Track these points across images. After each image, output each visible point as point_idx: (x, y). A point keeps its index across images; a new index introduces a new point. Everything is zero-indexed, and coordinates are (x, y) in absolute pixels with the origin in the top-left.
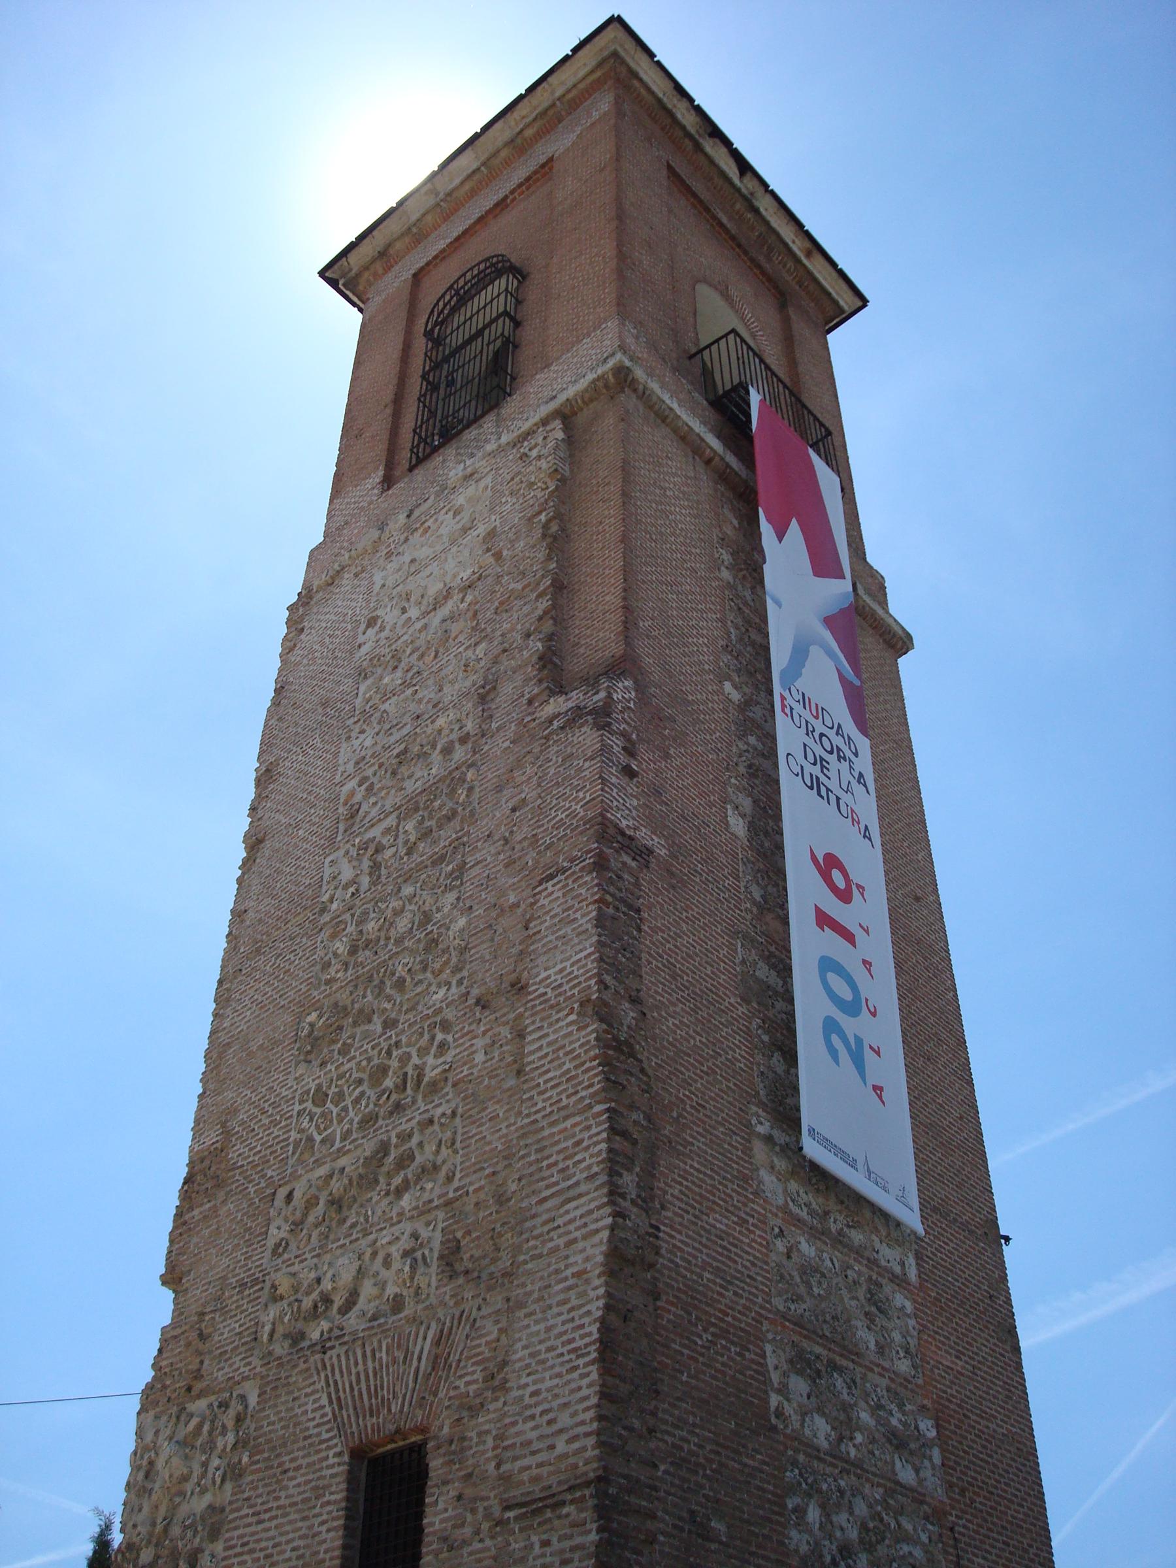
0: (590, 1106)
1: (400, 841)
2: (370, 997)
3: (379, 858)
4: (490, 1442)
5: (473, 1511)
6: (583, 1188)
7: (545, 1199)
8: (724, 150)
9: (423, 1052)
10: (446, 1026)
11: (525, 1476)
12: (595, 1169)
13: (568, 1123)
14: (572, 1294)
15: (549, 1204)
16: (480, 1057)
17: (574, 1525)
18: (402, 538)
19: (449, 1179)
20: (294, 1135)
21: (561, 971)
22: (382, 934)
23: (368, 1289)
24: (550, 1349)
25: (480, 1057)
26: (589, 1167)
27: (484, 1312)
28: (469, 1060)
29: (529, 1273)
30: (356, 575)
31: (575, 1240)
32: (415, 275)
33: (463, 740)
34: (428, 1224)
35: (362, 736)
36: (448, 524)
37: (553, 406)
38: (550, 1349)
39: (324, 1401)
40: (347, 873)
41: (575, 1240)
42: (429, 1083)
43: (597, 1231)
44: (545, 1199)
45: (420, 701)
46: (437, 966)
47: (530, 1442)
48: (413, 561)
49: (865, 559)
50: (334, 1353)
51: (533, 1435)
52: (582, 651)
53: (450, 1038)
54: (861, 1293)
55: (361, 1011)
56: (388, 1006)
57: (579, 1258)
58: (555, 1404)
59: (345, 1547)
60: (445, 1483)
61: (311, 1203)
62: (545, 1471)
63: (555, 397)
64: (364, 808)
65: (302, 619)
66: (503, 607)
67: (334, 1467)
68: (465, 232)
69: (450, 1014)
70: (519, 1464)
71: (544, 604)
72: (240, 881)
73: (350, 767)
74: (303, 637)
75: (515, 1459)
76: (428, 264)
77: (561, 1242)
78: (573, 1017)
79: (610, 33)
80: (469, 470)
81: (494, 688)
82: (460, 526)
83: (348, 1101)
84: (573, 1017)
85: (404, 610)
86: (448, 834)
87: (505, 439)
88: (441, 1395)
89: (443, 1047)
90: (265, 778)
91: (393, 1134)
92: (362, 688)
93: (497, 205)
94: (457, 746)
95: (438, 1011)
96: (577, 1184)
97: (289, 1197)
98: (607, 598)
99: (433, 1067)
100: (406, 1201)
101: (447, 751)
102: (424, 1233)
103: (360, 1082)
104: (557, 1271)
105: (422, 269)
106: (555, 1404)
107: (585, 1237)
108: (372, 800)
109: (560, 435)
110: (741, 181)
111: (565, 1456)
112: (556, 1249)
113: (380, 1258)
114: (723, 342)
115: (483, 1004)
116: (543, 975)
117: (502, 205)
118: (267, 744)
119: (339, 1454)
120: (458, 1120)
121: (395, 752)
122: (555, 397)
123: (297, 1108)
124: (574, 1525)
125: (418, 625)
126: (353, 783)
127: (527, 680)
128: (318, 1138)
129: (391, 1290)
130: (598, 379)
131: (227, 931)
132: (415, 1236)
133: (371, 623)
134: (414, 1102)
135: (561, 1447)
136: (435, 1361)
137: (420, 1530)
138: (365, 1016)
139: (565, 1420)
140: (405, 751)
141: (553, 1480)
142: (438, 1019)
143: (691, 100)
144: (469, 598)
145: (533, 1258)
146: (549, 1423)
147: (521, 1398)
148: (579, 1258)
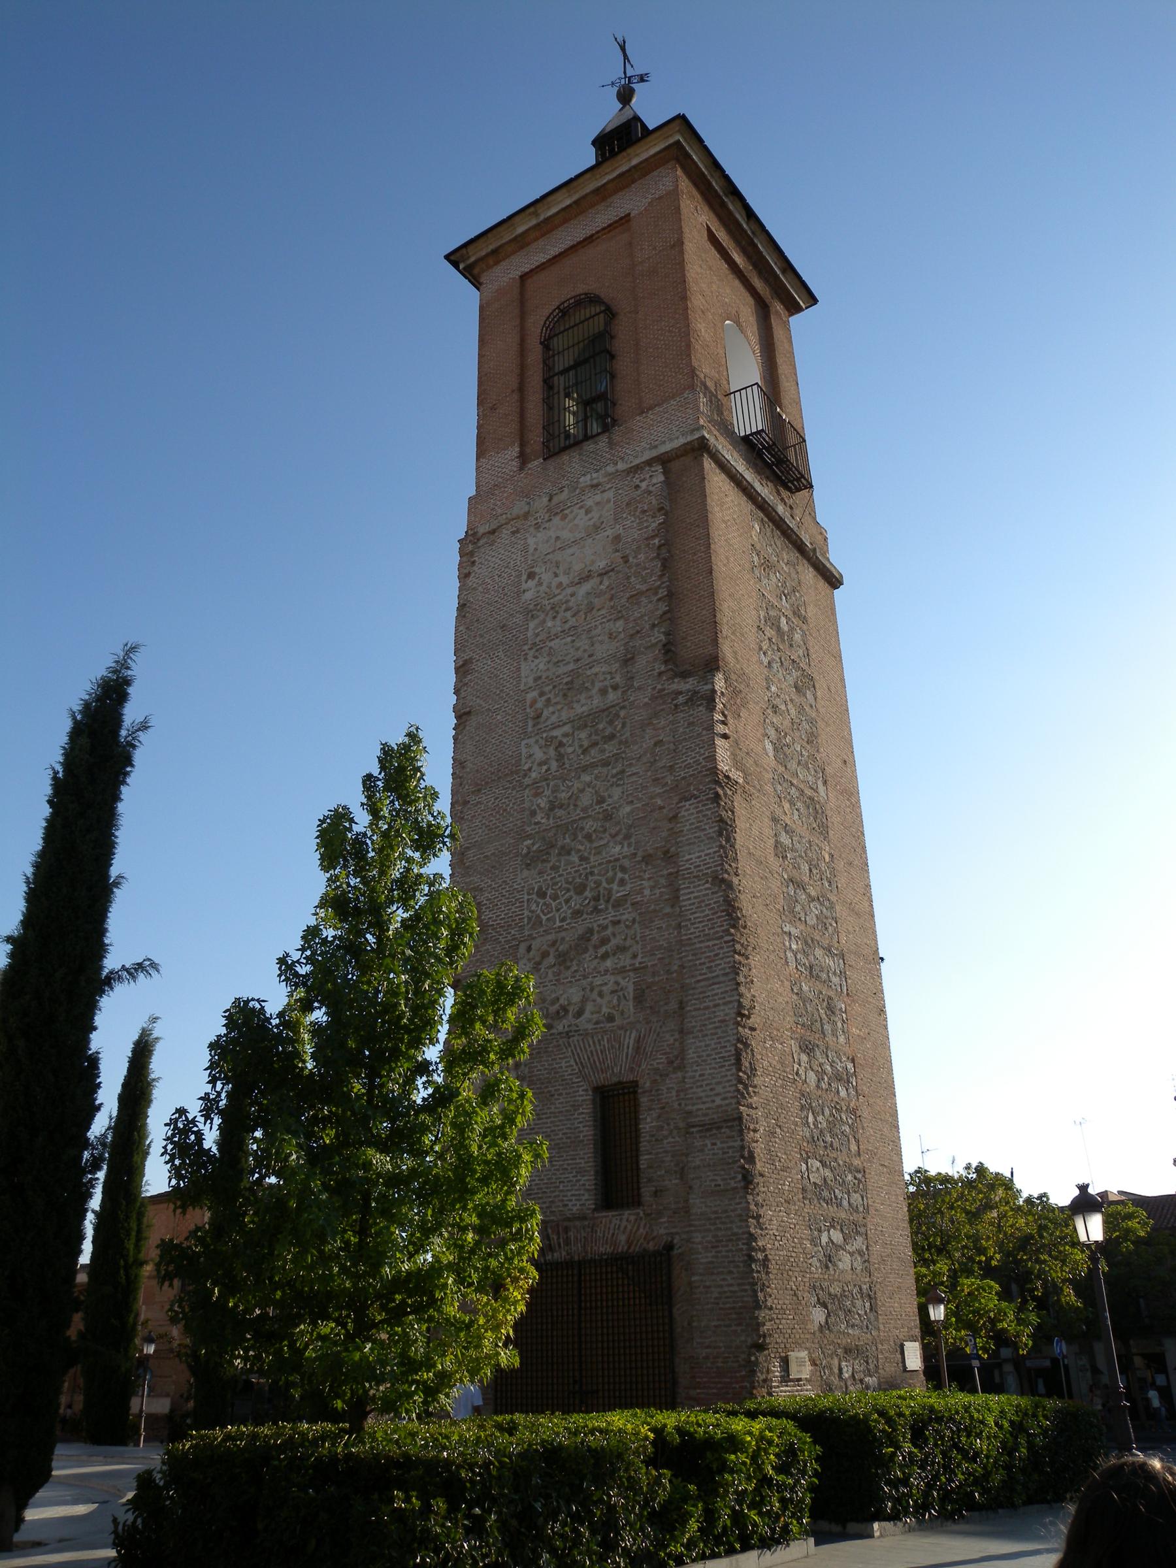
0: (722, 937)
1: (576, 743)
2: (568, 840)
3: (562, 750)
4: (674, 1093)
5: (668, 1124)
6: (722, 979)
7: (699, 981)
8: (739, 204)
9: (610, 881)
10: (623, 869)
11: (700, 1113)
12: (728, 970)
13: (710, 943)
14: (719, 1031)
15: (702, 984)
16: (647, 892)
17: (729, 1137)
18: (547, 518)
19: (635, 956)
20: (526, 913)
21: (699, 857)
22: (572, 801)
23: (589, 1007)
24: (708, 1055)
25: (647, 892)
26: (724, 969)
27: (664, 1029)
28: (640, 892)
29: (693, 1017)
30: (513, 533)
31: (718, 1005)
32: (521, 277)
33: (615, 688)
34: (624, 978)
35: (537, 661)
36: (582, 520)
37: (654, 453)
38: (708, 1055)
39: (572, 1062)
40: (539, 755)
41: (718, 1005)
42: (615, 901)
43: (731, 1002)
44: (699, 981)
45: (577, 649)
46: (613, 832)
47: (700, 1098)
48: (558, 538)
49: (814, 518)
50: (575, 1038)
51: (702, 1094)
52: (689, 644)
53: (626, 876)
54: (825, 1004)
55: (563, 847)
56: (580, 847)
57: (722, 1013)
58: (714, 1081)
59: (595, 1135)
60: (650, 1109)
61: (545, 955)
62: (710, 1112)
63: (656, 447)
64: (545, 713)
65: (471, 554)
66: (635, 598)
67: (584, 1096)
68: (561, 254)
69: (626, 863)
70: (695, 1108)
71: (663, 607)
72: (455, 738)
73: (531, 680)
74: (475, 568)
75: (693, 1105)
76: (532, 271)
77: (711, 1004)
78: (707, 885)
79: (676, 126)
80: (595, 482)
81: (633, 658)
82: (591, 523)
83: (562, 900)
84: (707, 885)
85: (556, 575)
86: (611, 748)
87: (621, 466)
88: (643, 1067)
89: (622, 882)
90: (462, 669)
91: (595, 925)
92: (532, 625)
93: (585, 240)
94: (610, 690)
95: (617, 860)
96: (717, 976)
97: (529, 949)
98: (704, 612)
99: (618, 892)
100: (609, 963)
101: (603, 692)
102: (623, 983)
103: (568, 890)
104: (710, 1018)
105: (527, 273)
106: (714, 1081)
107: (724, 1004)
108: (551, 709)
109: (662, 478)
110: (748, 224)
111: (719, 1106)
112: (707, 1008)
113: (596, 992)
114: (749, 390)
115: (648, 859)
116: (688, 857)
117: (589, 240)
118: (460, 647)
119: (586, 1090)
120: (636, 925)
121: (565, 681)
122: (656, 447)
123: (526, 897)
124: (729, 1137)
125: (569, 591)
126: (535, 694)
127: (655, 660)
128: (544, 918)
129: (605, 1010)
130: (687, 443)
131: (451, 771)
132: (617, 983)
133: (531, 576)
134: (607, 909)
135: (718, 1101)
136: (637, 1049)
137: (637, 1130)
138: (566, 851)
139: (719, 1089)
140: (572, 682)
141: (715, 1116)
142: (618, 864)
143: (723, 171)
144: (606, 583)
145: (696, 1010)
146: (711, 1090)
147: (694, 1077)
148: (722, 1013)
